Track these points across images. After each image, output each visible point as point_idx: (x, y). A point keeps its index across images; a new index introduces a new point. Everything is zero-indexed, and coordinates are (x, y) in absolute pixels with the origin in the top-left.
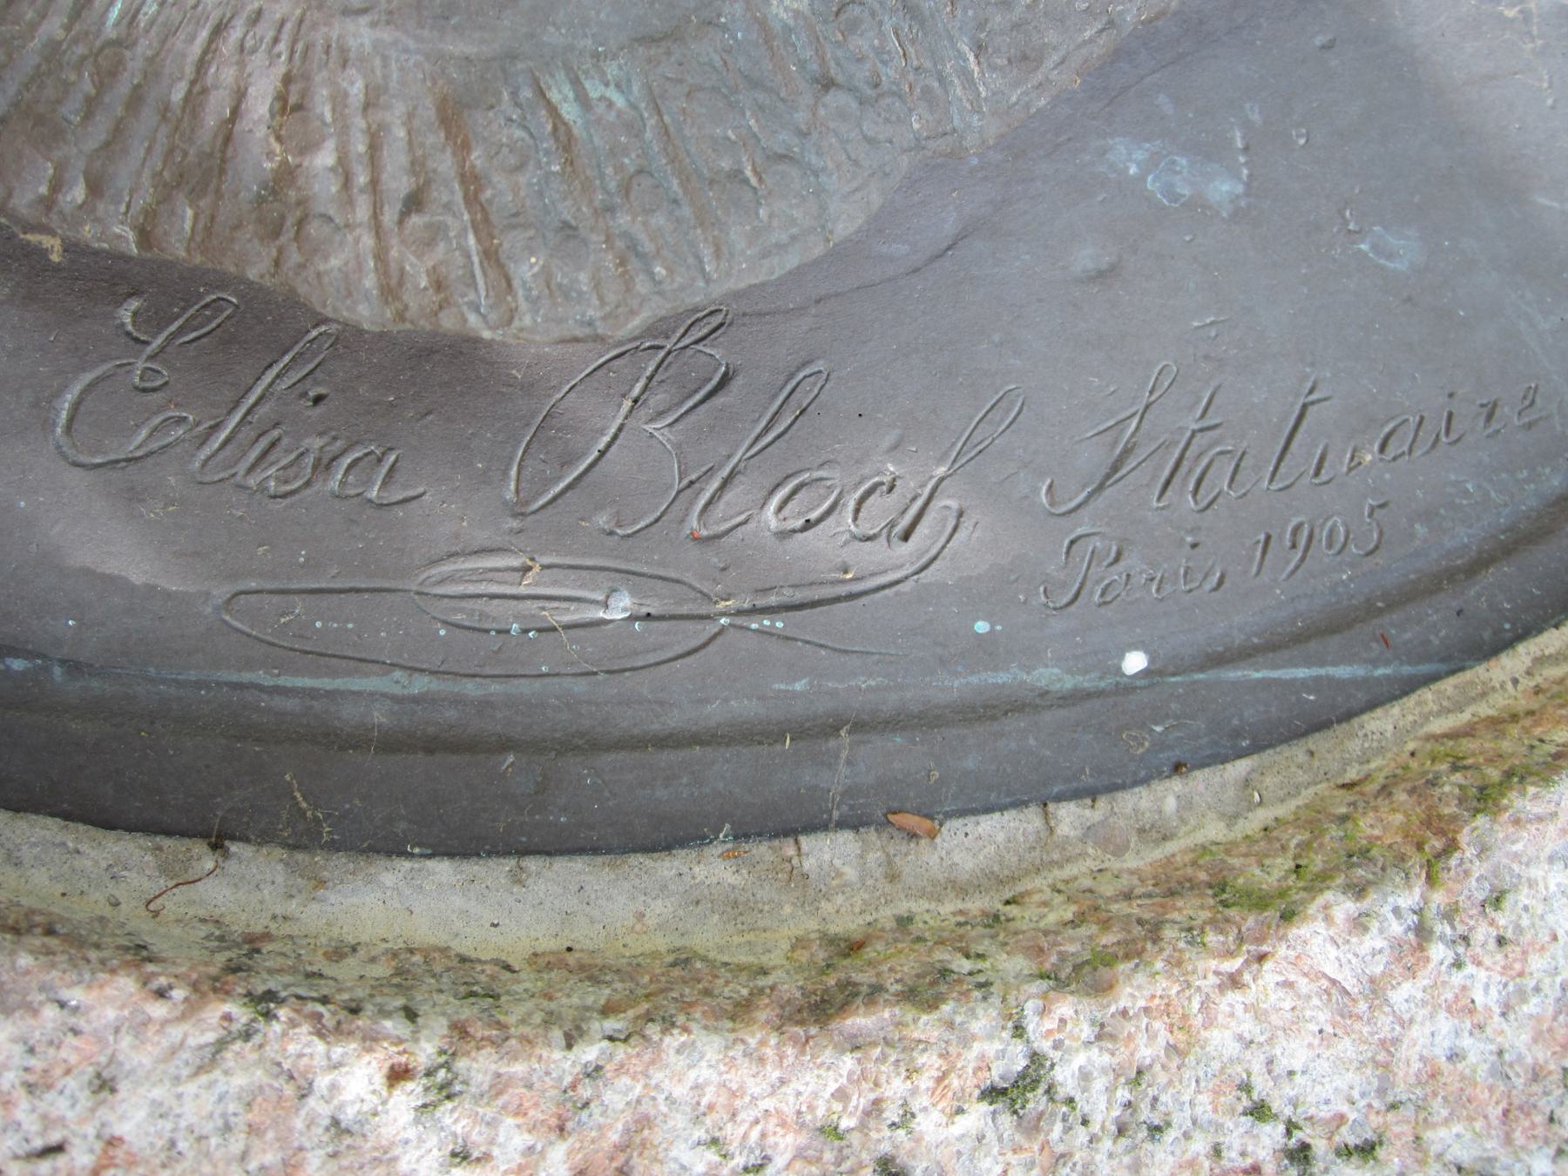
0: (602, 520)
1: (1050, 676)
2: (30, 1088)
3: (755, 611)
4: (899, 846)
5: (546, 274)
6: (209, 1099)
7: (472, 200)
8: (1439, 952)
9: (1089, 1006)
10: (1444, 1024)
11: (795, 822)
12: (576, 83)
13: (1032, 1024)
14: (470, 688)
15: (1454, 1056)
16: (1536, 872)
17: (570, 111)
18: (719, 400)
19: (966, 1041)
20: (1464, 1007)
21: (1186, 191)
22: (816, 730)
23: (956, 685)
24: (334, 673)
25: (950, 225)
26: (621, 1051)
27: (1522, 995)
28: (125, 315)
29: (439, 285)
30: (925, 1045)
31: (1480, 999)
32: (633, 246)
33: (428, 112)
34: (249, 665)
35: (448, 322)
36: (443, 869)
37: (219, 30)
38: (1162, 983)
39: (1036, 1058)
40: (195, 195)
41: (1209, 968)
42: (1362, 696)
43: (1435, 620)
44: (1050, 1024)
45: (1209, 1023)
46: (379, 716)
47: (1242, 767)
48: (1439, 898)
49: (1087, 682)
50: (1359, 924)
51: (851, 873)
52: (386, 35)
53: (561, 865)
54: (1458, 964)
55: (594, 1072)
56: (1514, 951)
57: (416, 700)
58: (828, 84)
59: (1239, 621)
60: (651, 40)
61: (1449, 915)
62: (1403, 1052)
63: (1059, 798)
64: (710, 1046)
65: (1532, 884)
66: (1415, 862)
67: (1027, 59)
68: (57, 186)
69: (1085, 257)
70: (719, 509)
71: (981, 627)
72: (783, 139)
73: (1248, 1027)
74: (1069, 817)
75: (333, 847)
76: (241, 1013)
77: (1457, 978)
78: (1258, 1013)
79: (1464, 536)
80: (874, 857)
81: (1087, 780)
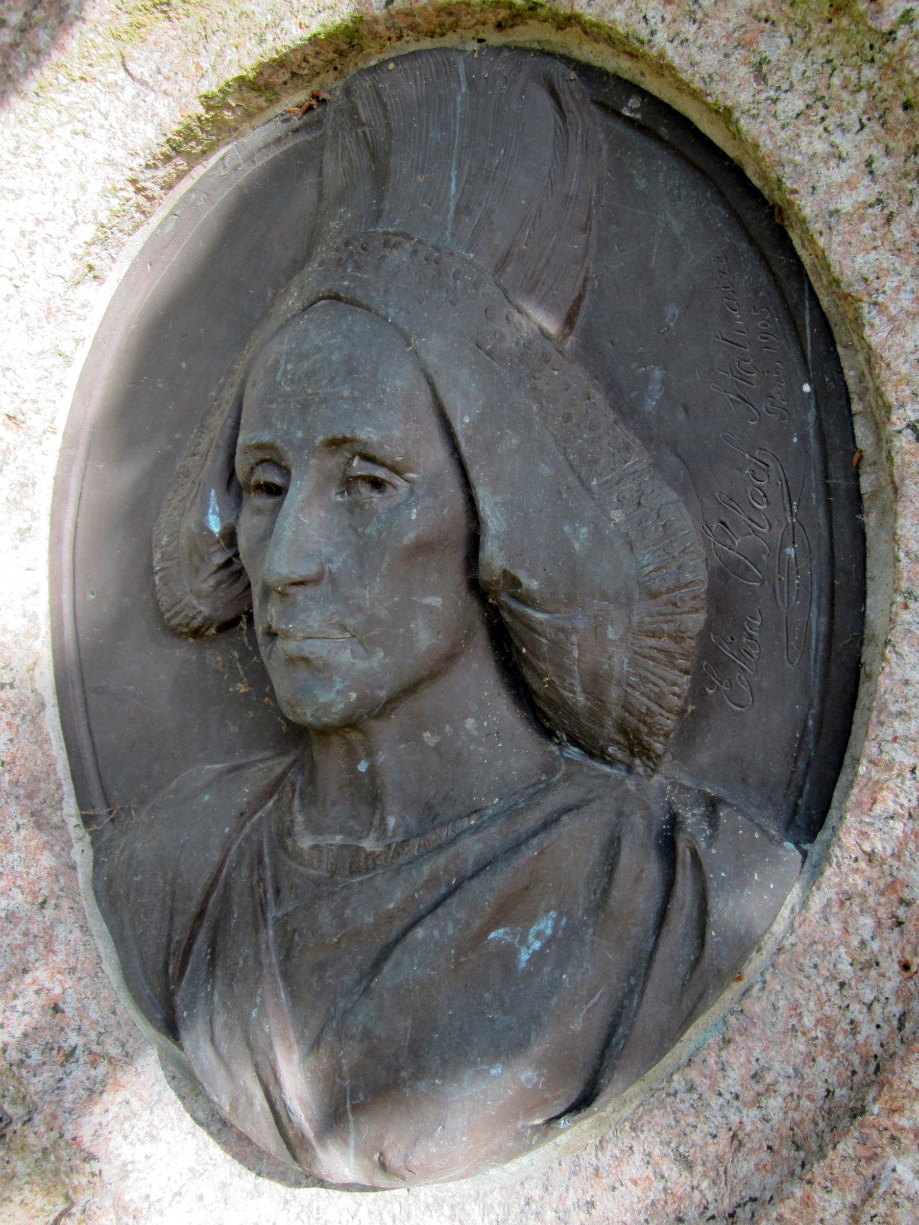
0: (765, 557)
1: (811, 416)
2: (906, 701)
3: (791, 511)
4: (865, 462)
5: (690, 572)
6: (911, 656)
7: (673, 591)
8: (880, 299)
9: (894, 411)
10: (902, 296)
11: (858, 497)
12: (643, 567)
13: (898, 428)
14: (815, 594)
15: (913, 292)
16: (857, 267)
17: (651, 568)
18: (728, 524)
19: (902, 448)
20: (898, 289)
21: (659, 386)
22: (828, 490)
23: (813, 445)
24: (811, 634)
25: (674, 458)
26: (902, 546)
27: (895, 269)
28: (711, 692)
29: (694, 598)
30: (902, 459)
31: (895, 284)
32: (683, 551)
33: (653, 602)
34: (809, 657)
35: (703, 596)
36: (869, 601)
37: (636, 653)
38: (889, 388)
39: (908, 426)
40: (676, 659)
41: (885, 374)
42: (816, 311)
43: (790, 286)
44: (898, 422)
45: (899, 373)
46: (824, 620)
47: (840, 349)
48: (865, 298)
49: (813, 403)
50: (872, 326)
51: (873, 477)
52: (635, 612)
53: (869, 565)
54: (884, 292)
55: (907, 554)
56: (881, 274)
57: (819, 610)
58: (639, 504)
59: (793, 354)
60: (632, 549)
61: (870, 295)
62: (910, 309)
63: (850, 410)
64: (901, 521)
65: (861, 268)
66: (857, 305)
67: (628, 448)
68: (675, 694)
69: (681, 416)
70: (761, 523)
71: (795, 440)
72: (654, 515)
73: (901, 360)
74: (856, 407)
75: (862, 632)
76: (889, 648)
77: (889, 292)
78: (898, 357)
79: (763, 278)
80: (868, 469)
81: (843, 402)
